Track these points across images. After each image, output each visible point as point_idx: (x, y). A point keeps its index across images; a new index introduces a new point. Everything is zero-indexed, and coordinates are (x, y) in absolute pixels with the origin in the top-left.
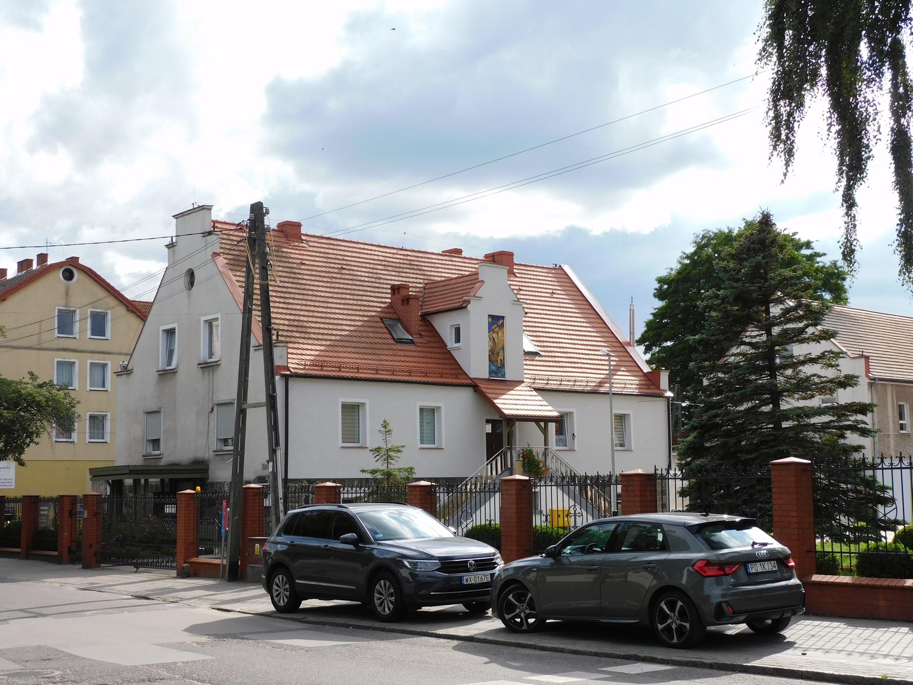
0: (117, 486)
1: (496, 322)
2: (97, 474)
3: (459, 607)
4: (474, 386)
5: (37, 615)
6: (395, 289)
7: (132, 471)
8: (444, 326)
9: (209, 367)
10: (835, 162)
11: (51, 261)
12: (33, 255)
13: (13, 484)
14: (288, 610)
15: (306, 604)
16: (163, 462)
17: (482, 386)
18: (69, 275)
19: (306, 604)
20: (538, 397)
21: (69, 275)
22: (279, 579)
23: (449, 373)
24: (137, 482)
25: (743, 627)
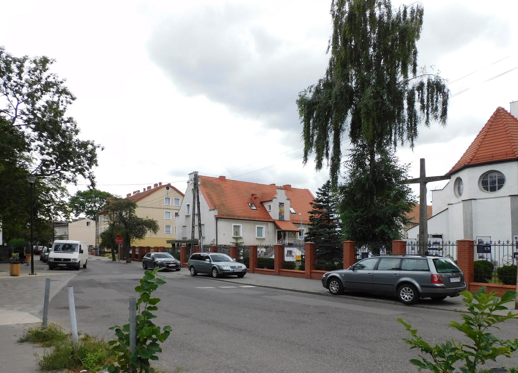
0: (173, 245)
1: (281, 204)
2: (168, 242)
3: (236, 276)
4: (274, 222)
5: (181, 279)
6: (253, 195)
7: (177, 241)
8: (266, 205)
9: (187, 216)
10: (106, 192)
11: (162, 184)
12: (158, 183)
14: (195, 275)
15: (198, 274)
16: (187, 240)
17: (277, 222)
18: (168, 188)
19: (198, 274)
20: (294, 225)
21: (168, 188)
22: (192, 269)
23: (267, 219)
24: (178, 244)
25: (429, 298)
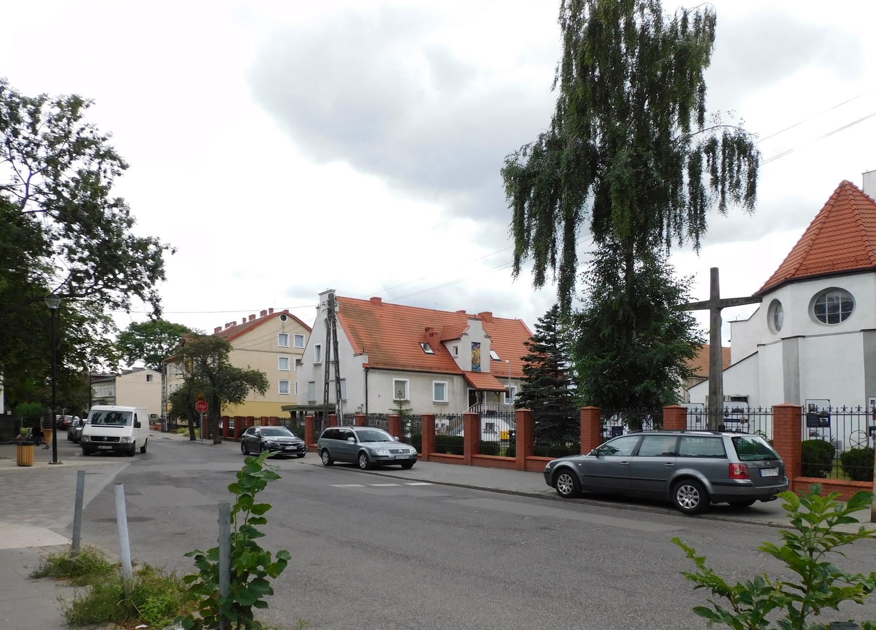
0: (293, 414)
1: (476, 345)
2: (285, 408)
3: (400, 466)
4: (463, 375)
6: (427, 329)
7: (299, 408)
8: (450, 347)
9: (317, 365)
10: (180, 324)
11: (275, 311)
12: (267, 309)
13: (483, 426)
14: (330, 464)
15: (335, 463)
16: (317, 405)
17: (468, 375)
18: (284, 318)
19: (335, 463)
20: (496, 380)
21: (284, 318)
22: (325, 454)
23: (451, 370)
24: (301, 413)
